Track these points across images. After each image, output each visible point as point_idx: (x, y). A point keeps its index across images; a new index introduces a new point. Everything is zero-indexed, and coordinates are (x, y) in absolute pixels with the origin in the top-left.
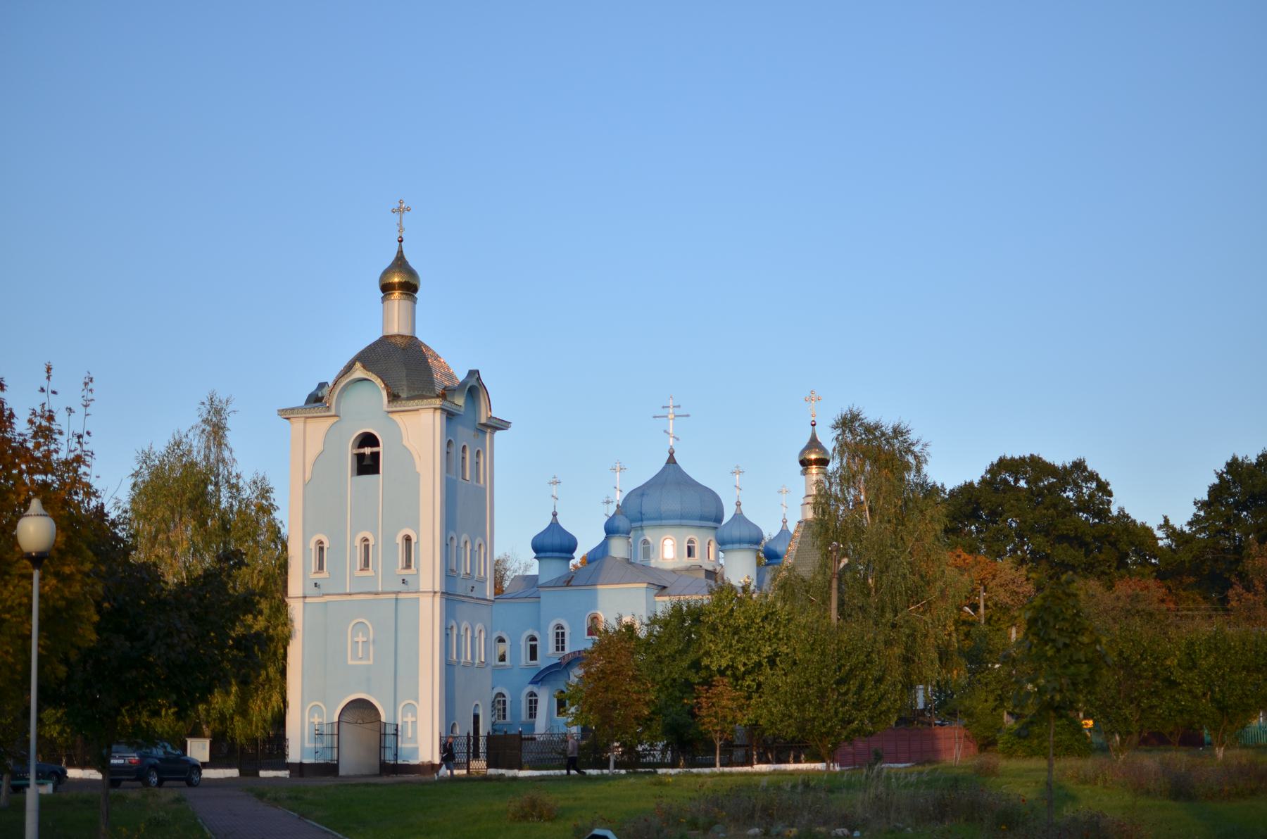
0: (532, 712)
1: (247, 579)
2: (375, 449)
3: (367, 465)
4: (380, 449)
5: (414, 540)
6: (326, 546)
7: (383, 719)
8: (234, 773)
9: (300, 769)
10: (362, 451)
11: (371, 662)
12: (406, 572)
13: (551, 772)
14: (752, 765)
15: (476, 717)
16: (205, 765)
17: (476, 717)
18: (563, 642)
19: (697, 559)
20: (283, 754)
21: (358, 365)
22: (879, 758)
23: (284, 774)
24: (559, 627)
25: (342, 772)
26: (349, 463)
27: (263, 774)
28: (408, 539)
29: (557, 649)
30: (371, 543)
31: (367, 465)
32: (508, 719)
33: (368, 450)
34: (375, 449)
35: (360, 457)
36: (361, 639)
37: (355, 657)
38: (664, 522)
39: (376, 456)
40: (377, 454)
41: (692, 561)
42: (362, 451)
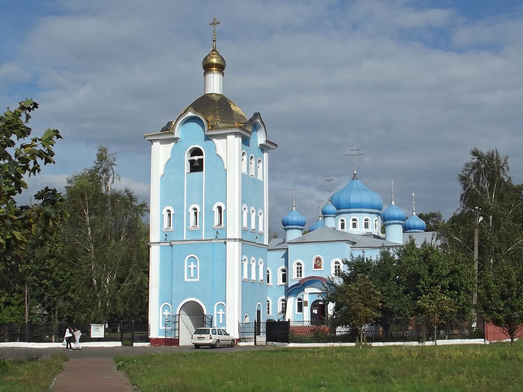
0: (284, 311)
1: (118, 184)
2: (201, 157)
3: (196, 167)
4: (204, 157)
5: (223, 209)
6: (172, 213)
7: (205, 313)
8: (119, 344)
9: (156, 342)
10: (193, 158)
11: (198, 280)
12: (219, 227)
13: (328, 345)
14: (422, 342)
15: (259, 312)
16: (239, 340)
17: (259, 312)
18: (301, 272)
19: (369, 230)
20: (144, 325)
21: (190, 109)
22: (133, 340)
23: (147, 344)
24: (299, 264)
25: (181, 344)
26: (187, 166)
27: (135, 344)
28: (220, 208)
29: (298, 276)
30: (198, 211)
31: (196, 167)
32: (271, 313)
33: (196, 158)
34: (201, 157)
35: (192, 162)
36: (192, 266)
37: (189, 277)
38: (352, 210)
39: (201, 161)
40: (202, 159)
41: (367, 230)
42: (193, 158)
